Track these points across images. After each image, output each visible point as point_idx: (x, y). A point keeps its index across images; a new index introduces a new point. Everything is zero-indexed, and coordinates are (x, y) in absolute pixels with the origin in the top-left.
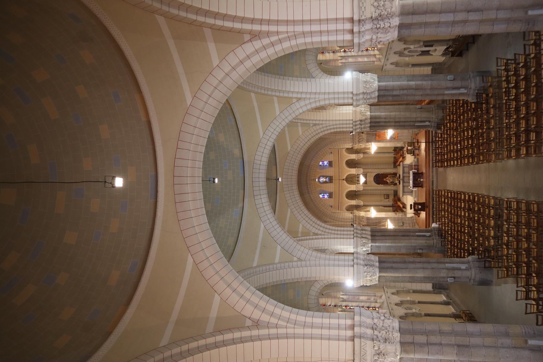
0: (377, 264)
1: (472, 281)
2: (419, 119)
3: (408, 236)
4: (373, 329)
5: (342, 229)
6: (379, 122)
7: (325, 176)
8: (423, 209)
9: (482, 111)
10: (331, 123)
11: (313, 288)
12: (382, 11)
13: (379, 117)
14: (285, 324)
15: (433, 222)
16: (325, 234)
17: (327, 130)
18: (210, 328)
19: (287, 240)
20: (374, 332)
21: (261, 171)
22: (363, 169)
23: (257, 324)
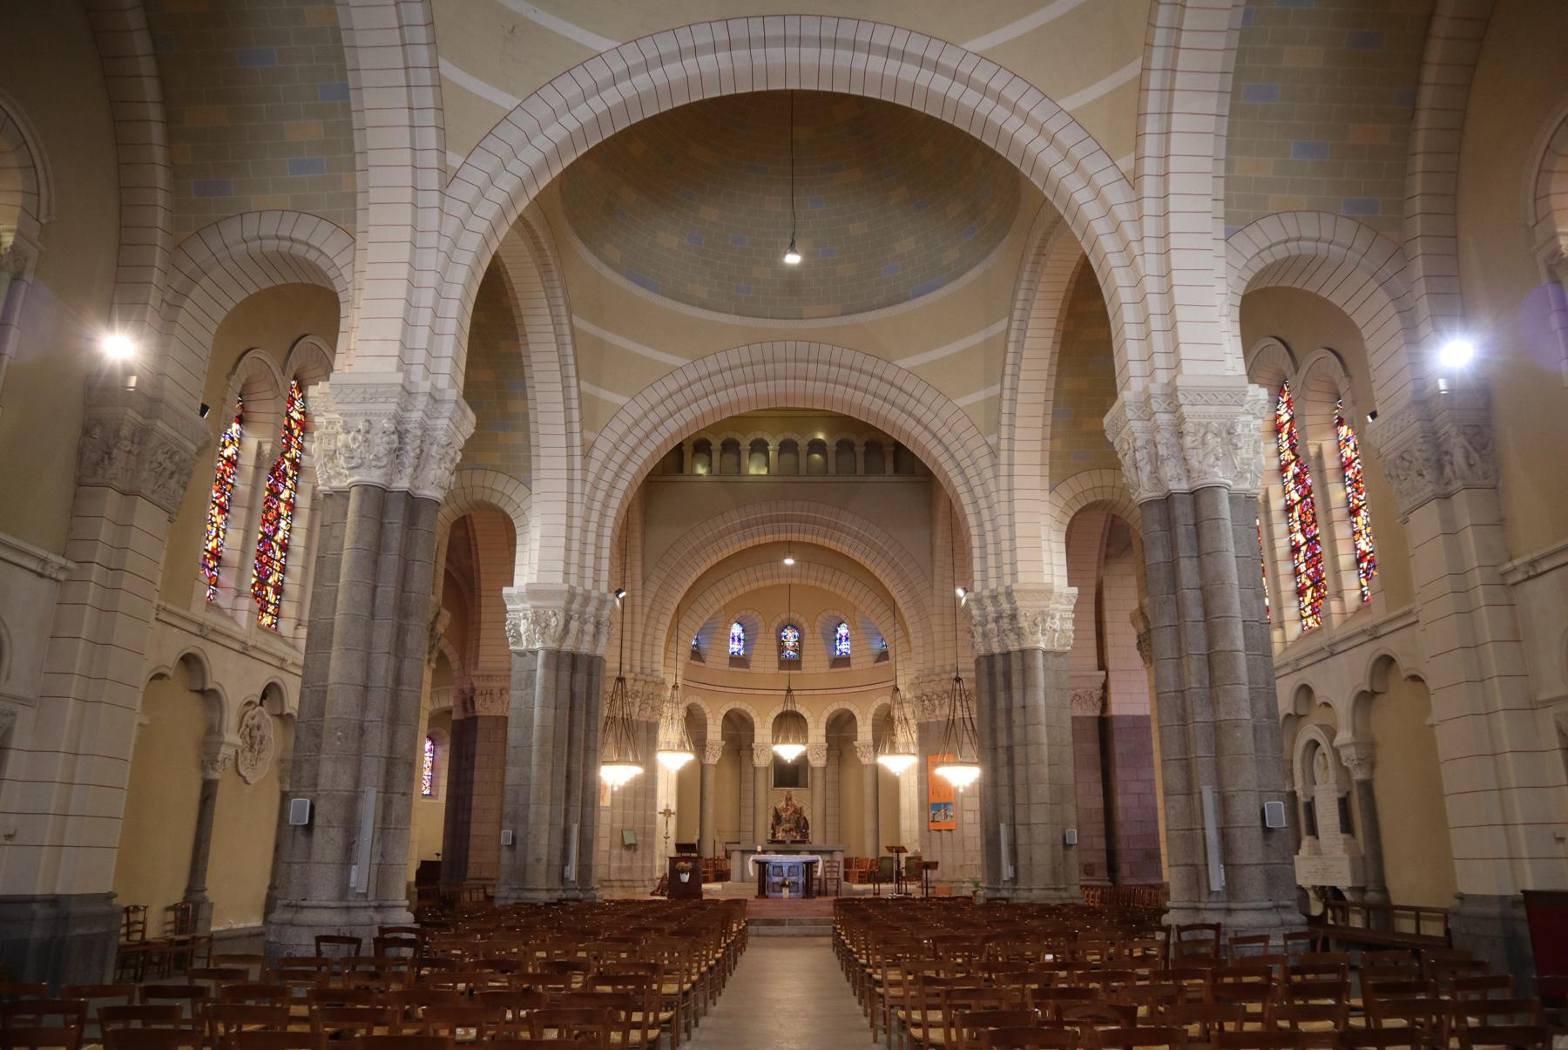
0: (402, 484)
3: (568, 793)
6: (1008, 687)
7: (800, 646)
9: (1305, 555)
10: (1002, 508)
11: (326, 227)
13: (1027, 685)
16: (588, 486)
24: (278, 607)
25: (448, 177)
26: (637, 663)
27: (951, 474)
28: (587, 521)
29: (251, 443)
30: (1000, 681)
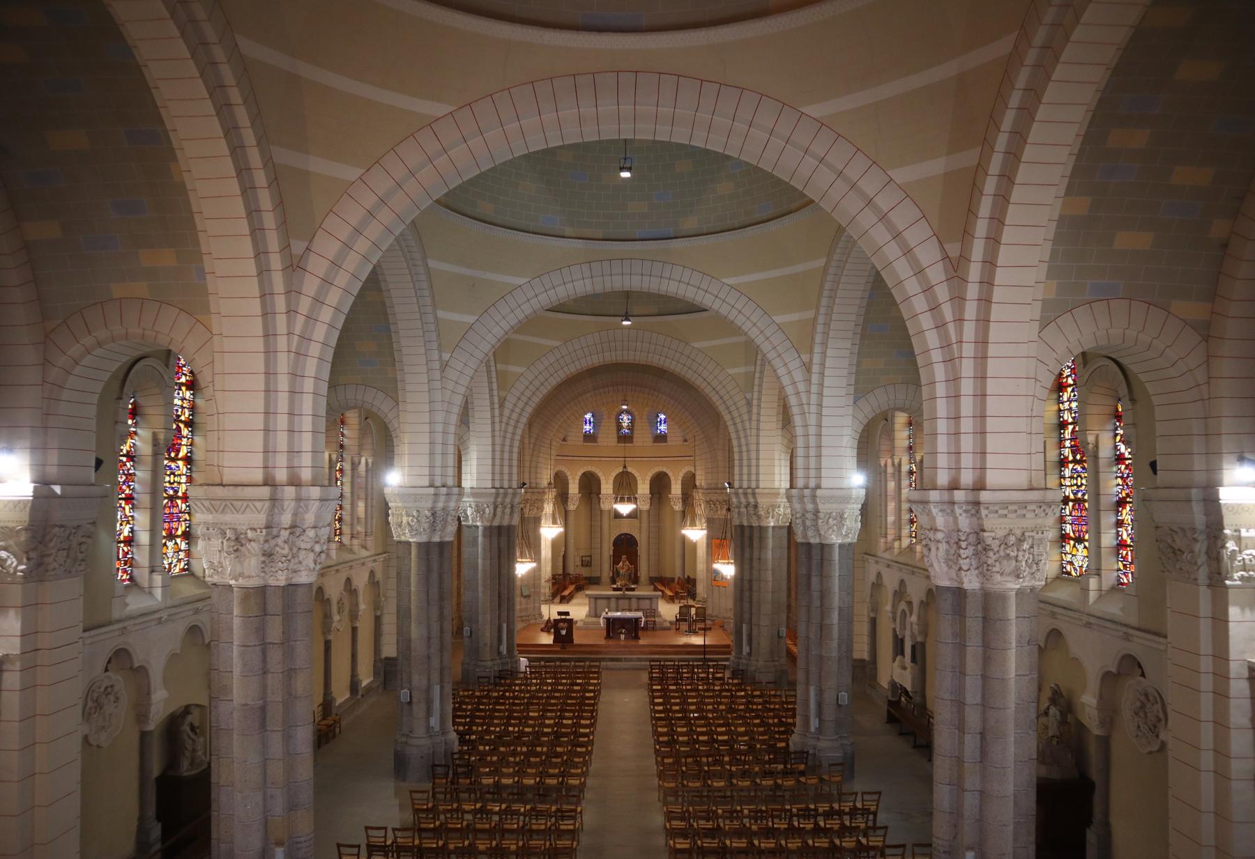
0: (436, 539)
1: (404, 739)
2: (755, 632)
5: (515, 463)
6: (751, 546)
7: (633, 426)
8: (558, 638)
10: (753, 440)
11: (381, 395)
12: (995, 554)
13: (762, 547)
14: (298, 330)
15: (530, 660)
16: (503, 425)
17: (737, 431)
18: (283, 156)
20: (286, 529)
21: (646, 279)
23: (295, 267)
28: (503, 445)
30: (747, 543)
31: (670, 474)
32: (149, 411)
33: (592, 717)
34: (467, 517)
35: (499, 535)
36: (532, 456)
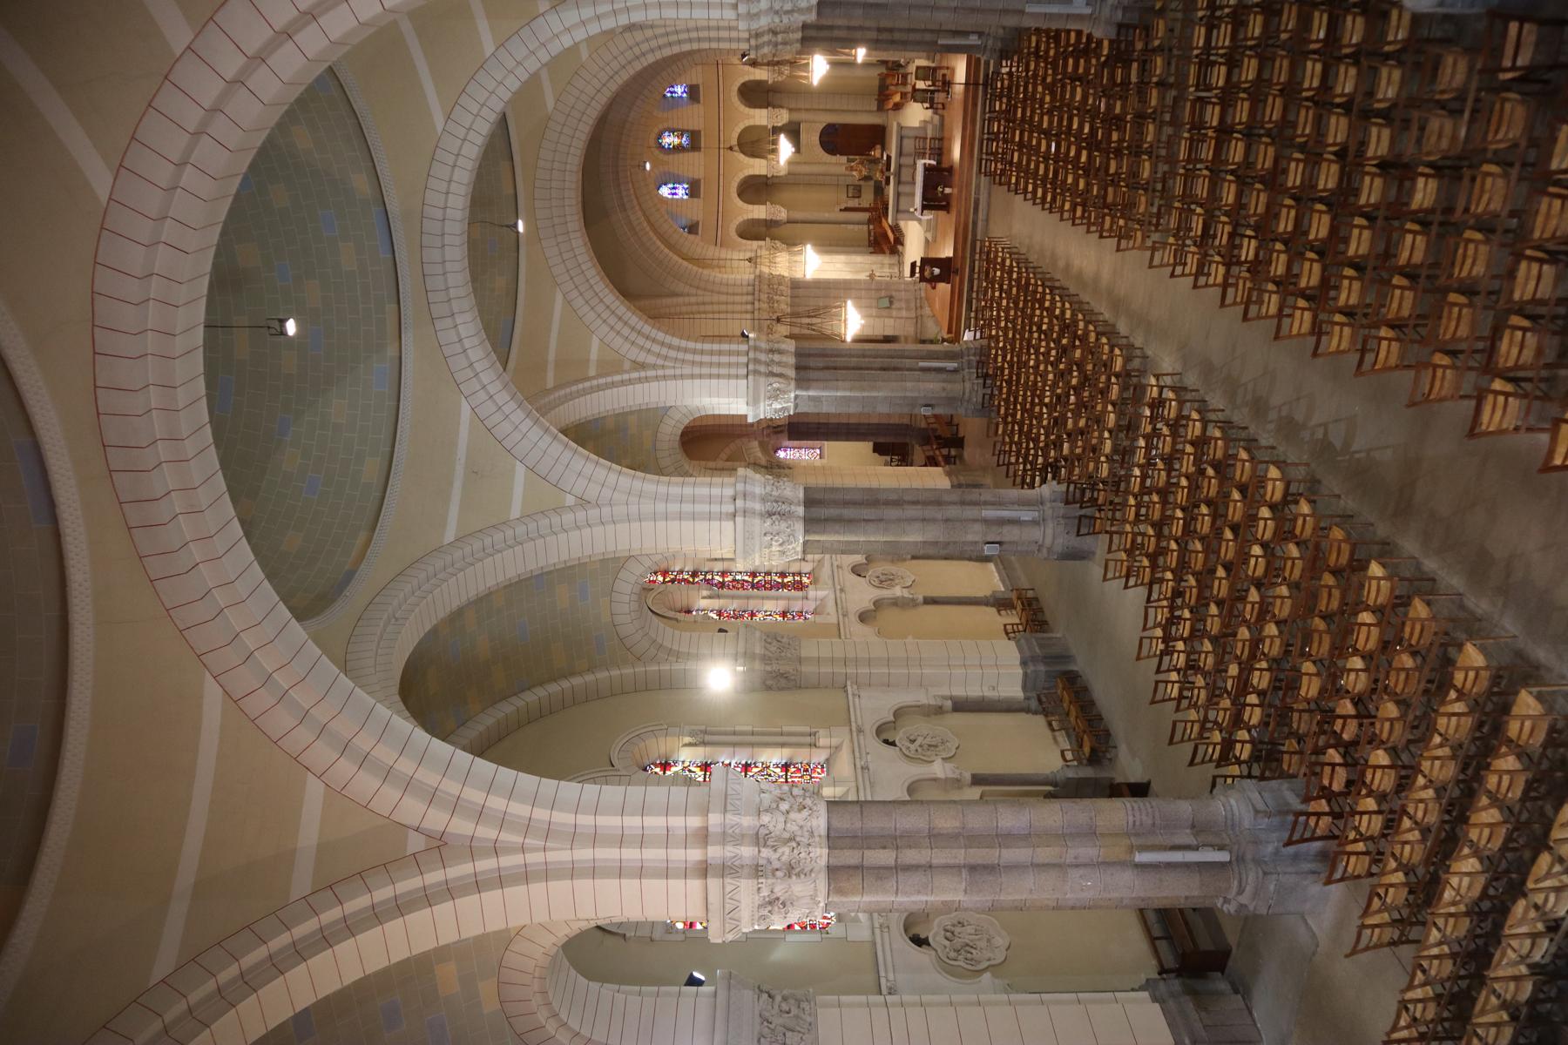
0: (801, 510)
3: (895, 369)
4: (757, 844)
8: (942, 278)
15: (968, 327)
16: (666, 363)
18: (302, 883)
19: (543, 445)
22: (791, 110)
23: (440, 847)
24: (794, 575)
25: (583, 502)
26: (745, 298)
27: (645, 64)
29: (703, 603)
31: (742, 80)
32: (662, 750)
33: (1023, 482)
34: (783, 409)
35: (806, 368)
36: (712, 291)
